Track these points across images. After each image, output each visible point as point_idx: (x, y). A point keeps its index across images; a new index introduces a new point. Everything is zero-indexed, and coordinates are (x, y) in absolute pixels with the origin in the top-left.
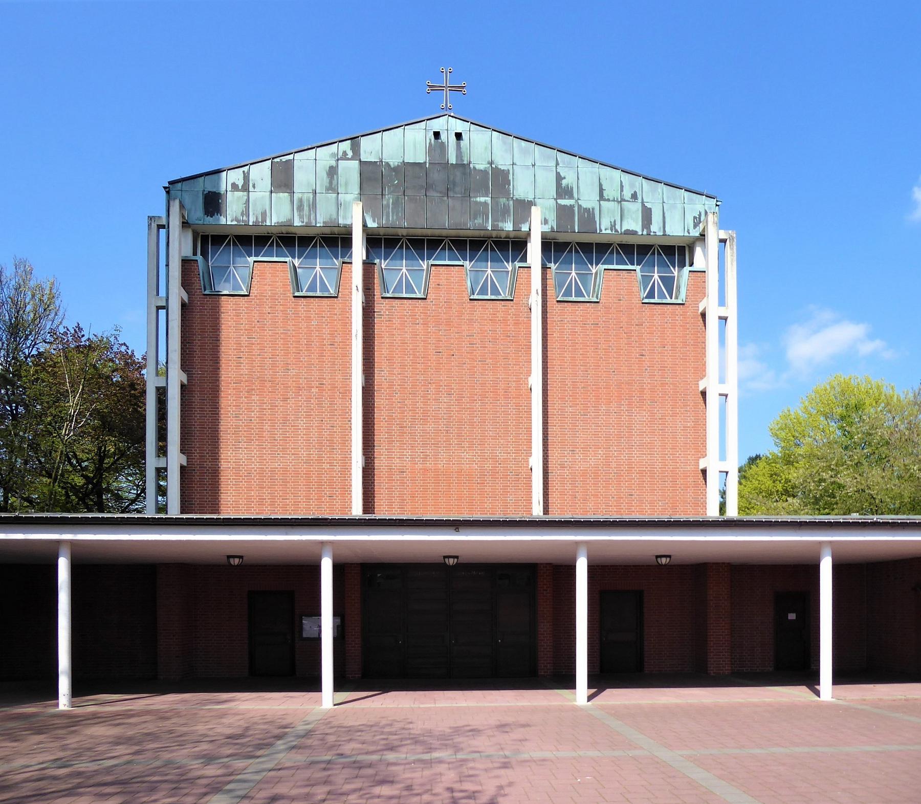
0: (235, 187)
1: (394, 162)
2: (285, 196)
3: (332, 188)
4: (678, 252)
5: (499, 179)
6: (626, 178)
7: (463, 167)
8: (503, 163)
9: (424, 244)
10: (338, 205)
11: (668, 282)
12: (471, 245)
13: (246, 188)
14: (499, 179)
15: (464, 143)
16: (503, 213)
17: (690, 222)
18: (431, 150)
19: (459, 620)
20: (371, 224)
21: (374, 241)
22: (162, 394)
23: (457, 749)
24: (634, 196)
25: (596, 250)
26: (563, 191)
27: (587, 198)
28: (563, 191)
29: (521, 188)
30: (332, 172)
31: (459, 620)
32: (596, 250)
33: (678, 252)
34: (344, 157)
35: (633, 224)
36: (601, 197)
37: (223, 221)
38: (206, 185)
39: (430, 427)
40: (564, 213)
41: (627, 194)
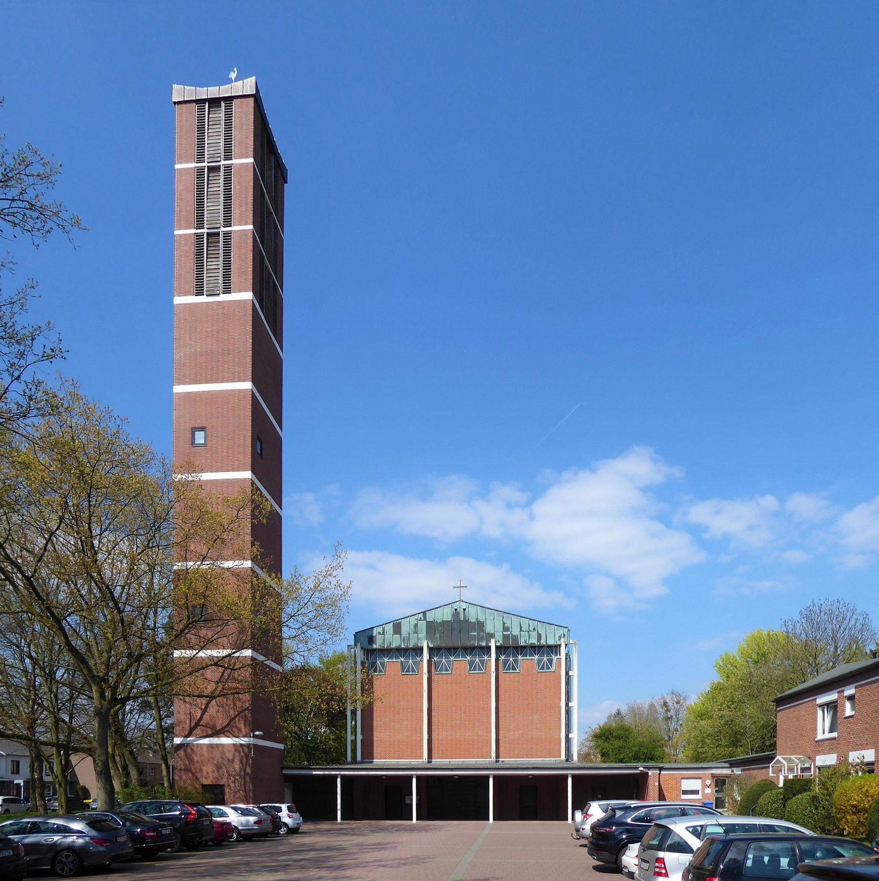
0: (379, 633)
1: (439, 621)
2: (398, 636)
3: (416, 632)
4: (554, 649)
5: (480, 625)
6: (531, 622)
7: (466, 621)
8: (482, 619)
9: (452, 650)
10: (418, 639)
11: (551, 661)
12: (469, 650)
13: (383, 634)
14: (480, 625)
15: (467, 612)
16: (482, 639)
17: (557, 638)
18: (453, 615)
19: (453, 798)
20: (431, 645)
21: (430, 650)
22: (354, 742)
23: (32, 686)
24: (534, 629)
25: (520, 650)
26: (506, 629)
27: (515, 631)
28: (506, 629)
29: (489, 629)
30: (416, 626)
31: (453, 798)
32: (520, 650)
33: (554, 649)
34: (420, 620)
35: (534, 641)
36: (521, 630)
37: (375, 646)
38: (367, 634)
39: (453, 723)
40: (506, 637)
41: (531, 629)
